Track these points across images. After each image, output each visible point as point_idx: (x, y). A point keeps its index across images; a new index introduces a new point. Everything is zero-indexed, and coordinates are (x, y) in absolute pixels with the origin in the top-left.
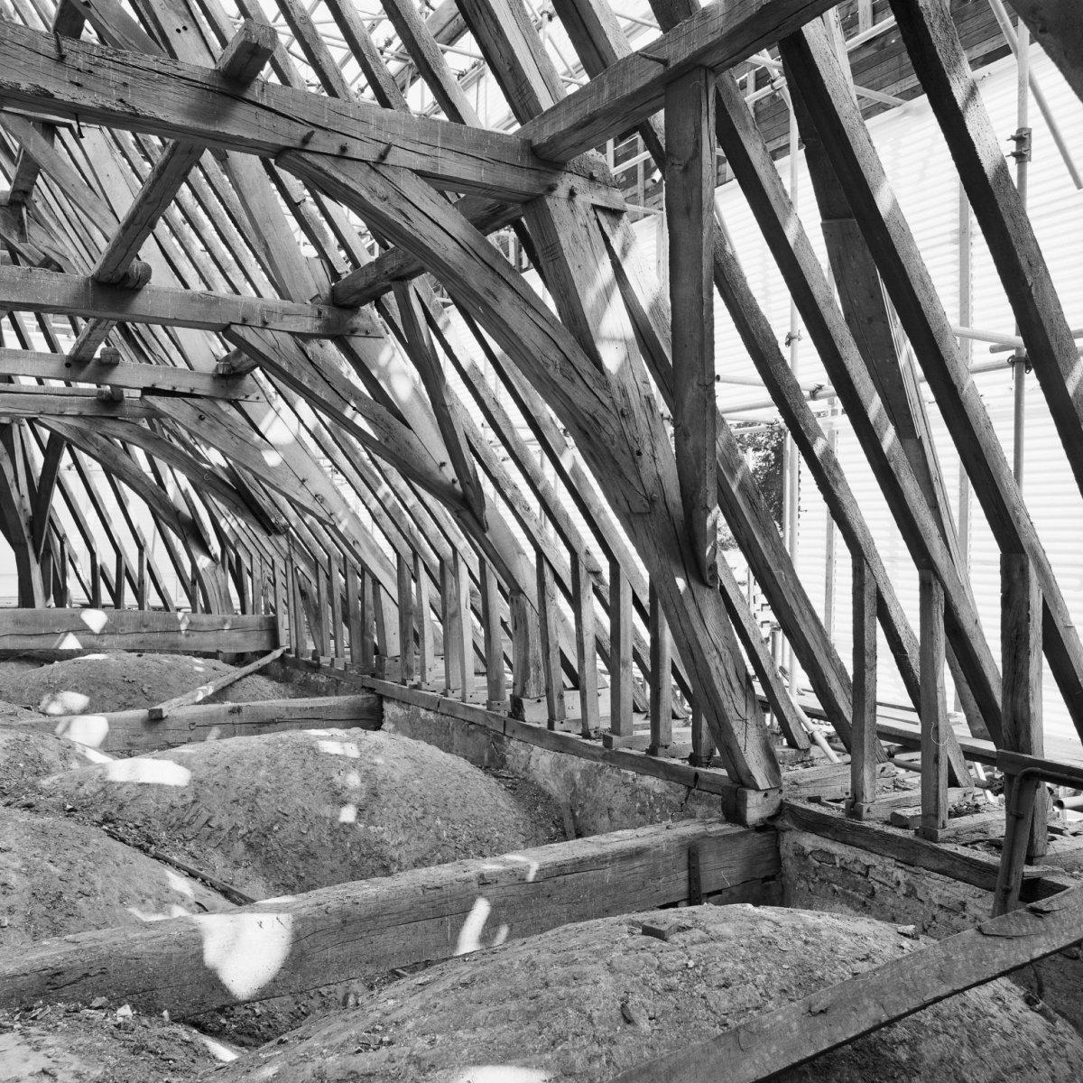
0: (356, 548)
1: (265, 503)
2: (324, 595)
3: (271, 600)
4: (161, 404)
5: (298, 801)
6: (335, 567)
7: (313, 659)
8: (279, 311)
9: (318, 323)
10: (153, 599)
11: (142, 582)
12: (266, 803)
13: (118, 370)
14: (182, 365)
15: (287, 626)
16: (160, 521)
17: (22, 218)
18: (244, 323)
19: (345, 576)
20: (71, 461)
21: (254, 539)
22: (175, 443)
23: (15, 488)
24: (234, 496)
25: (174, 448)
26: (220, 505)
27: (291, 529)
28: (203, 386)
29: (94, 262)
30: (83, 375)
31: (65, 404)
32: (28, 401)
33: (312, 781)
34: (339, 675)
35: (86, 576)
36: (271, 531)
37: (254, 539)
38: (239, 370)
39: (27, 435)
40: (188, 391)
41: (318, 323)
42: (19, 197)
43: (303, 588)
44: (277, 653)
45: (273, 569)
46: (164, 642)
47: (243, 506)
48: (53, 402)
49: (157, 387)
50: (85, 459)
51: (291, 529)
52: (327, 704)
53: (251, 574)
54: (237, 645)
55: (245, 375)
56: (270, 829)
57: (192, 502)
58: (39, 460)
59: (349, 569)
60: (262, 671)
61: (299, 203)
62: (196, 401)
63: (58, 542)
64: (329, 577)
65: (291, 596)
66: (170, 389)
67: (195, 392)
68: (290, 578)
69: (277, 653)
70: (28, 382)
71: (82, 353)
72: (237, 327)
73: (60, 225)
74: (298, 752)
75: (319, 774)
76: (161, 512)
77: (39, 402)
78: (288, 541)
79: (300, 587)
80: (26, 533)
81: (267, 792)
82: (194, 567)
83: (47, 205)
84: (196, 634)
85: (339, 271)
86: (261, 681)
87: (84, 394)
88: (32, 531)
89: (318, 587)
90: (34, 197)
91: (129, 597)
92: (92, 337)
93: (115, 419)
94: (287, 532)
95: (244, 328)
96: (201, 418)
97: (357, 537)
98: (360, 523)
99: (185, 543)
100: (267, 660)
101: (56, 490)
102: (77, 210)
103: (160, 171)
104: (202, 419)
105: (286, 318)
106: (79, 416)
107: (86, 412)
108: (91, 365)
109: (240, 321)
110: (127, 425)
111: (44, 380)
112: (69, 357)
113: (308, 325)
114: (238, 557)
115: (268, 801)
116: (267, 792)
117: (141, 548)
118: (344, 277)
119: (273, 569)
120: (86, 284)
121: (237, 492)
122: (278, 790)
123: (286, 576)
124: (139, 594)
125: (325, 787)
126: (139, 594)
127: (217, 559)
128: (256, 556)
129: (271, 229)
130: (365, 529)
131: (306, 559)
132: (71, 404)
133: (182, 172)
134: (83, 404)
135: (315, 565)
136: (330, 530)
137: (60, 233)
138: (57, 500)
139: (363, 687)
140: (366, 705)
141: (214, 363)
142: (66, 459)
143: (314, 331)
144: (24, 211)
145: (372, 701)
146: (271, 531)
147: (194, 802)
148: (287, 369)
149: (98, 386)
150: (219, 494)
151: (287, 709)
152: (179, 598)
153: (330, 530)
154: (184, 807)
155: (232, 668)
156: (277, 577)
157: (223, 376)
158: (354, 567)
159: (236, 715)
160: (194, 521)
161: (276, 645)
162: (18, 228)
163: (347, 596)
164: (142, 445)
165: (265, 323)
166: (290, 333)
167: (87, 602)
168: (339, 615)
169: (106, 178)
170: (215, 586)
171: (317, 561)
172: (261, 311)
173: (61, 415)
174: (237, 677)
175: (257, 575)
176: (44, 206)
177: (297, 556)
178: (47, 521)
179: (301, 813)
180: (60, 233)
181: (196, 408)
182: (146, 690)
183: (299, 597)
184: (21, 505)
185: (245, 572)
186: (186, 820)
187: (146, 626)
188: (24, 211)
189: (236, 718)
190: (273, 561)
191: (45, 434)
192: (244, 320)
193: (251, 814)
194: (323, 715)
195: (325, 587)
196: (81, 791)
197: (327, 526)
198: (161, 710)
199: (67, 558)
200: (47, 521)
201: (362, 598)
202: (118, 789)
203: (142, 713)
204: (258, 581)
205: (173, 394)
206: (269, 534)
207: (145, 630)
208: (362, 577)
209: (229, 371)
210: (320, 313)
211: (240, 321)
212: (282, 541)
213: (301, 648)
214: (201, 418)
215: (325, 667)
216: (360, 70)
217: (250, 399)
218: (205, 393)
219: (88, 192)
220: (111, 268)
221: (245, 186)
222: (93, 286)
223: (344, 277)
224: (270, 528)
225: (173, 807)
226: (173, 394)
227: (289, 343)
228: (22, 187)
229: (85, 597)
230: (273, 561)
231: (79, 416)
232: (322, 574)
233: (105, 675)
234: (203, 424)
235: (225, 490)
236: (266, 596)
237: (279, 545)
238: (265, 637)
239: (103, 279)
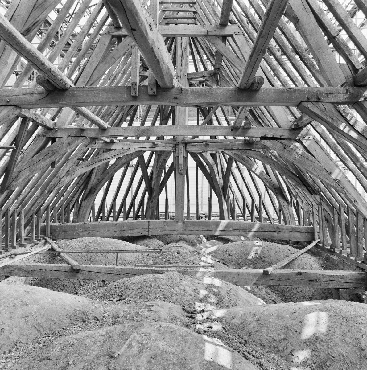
0: (356, 204)
1: (310, 181)
2: (337, 221)
3: (311, 220)
4: (267, 143)
5: (340, 349)
6: (342, 210)
7: (331, 248)
8: (326, 92)
9: (346, 96)
10: (264, 215)
11: (261, 210)
12: (322, 347)
13: (251, 130)
14: (275, 126)
15: (318, 231)
16: (267, 187)
17: (218, 79)
18: (308, 100)
19: (348, 215)
20: (236, 166)
21: (304, 195)
22: (273, 158)
23: (218, 176)
24: (297, 179)
25: (273, 160)
26: (290, 182)
27: (321, 192)
28: (285, 134)
29: (238, 83)
30: (237, 133)
31: (233, 145)
32: (221, 145)
33: (347, 339)
34: (345, 259)
35: (241, 206)
36: (313, 193)
37: (304, 195)
38: (301, 126)
39: (222, 157)
40: (279, 137)
41: (346, 96)
42: (217, 71)
43: (327, 218)
44: (314, 244)
45: (312, 208)
46: (269, 235)
47: (301, 183)
48: (228, 145)
49: (267, 136)
50: (241, 165)
51: (321, 192)
52: (341, 275)
53: (303, 209)
54: (297, 238)
55: (303, 128)
56: (325, 363)
57: (279, 180)
58: (225, 165)
59: (350, 212)
60: (309, 251)
61: (336, 37)
62: (283, 141)
63: (232, 194)
64: (339, 215)
65: (321, 219)
66: (272, 136)
67: (275, 136)
68: (320, 212)
69: (314, 244)
70: (221, 138)
71: (237, 125)
72: (305, 102)
73: (231, 79)
74: (337, 318)
75: (350, 335)
76: (268, 184)
77: (224, 145)
78: (320, 197)
79: (325, 217)
80: (221, 192)
81: (322, 341)
82: (280, 205)
83: (226, 73)
84: (281, 233)
85: (358, 68)
86: (308, 256)
87: (240, 141)
88: (223, 191)
89: (334, 218)
90: (222, 71)
91: (256, 214)
92: (240, 117)
93: (250, 150)
94: (320, 194)
95: (308, 103)
96: (285, 148)
97: (356, 199)
98: (358, 192)
99: (277, 196)
100: (310, 247)
101: (231, 176)
102: (232, 66)
103: (267, 40)
104: (285, 148)
105: (329, 96)
106: (238, 149)
107: (240, 148)
108: (240, 129)
109: (306, 100)
110: (256, 152)
111: (227, 137)
112: (232, 127)
113: (342, 97)
114: (297, 202)
115: (323, 346)
116: (322, 341)
117: (260, 197)
118: (360, 71)
119: (312, 208)
120: (235, 91)
121: (298, 177)
122: (328, 340)
123: (318, 211)
124: (259, 213)
125: (354, 343)
126: (259, 213)
127: (289, 202)
128: (305, 201)
129: (321, 52)
130: (360, 195)
131: (328, 205)
132: (235, 145)
133: (281, 10)
134: (239, 145)
135: (332, 208)
136: (342, 196)
137: (231, 82)
138: (231, 179)
139: (358, 267)
140: (360, 277)
141: (289, 125)
142: (234, 165)
143: (344, 101)
144: (218, 76)
145: (363, 275)
146: (313, 193)
147: (284, 339)
148: (330, 121)
149: (245, 138)
150: (290, 177)
151: (322, 275)
152: (274, 216)
153: (342, 196)
154: (279, 341)
155: (296, 250)
156: (314, 211)
157: (294, 129)
158: (352, 211)
159: (299, 276)
160: (280, 187)
161: (314, 240)
162: (217, 83)
163: (349, 224)
164: (260, 159)
165: (319, 99)
166: (331, 103)
167: (241, 215)
168: (344, 231)
169: (245, 53)
170: (288, 213)
171: (333, 207)
172: (317, 93)
173: (231, 150)
174: (299, 255)
175: (305, 209)
176: (225, 73)
177: (324, 204)
178: (228, 187)
179: (342, 358)
180: (231, 82)
181: (282, 144)
182: (262, 257)
183: (324, 221)
184: (220, 182)
185: (300, 208)
186: (281, 349)
187: (262, 229)
188: (218, 76)
189: (299, 277)
190: (312, 205)
191: (227, 157)
192: (308, 99)
193: (314, 352)
194: (340, 280)
195: (337, 218)
196: (233, 321)
197: (341, 194)
198: (268, 271)
199: (235, 200)
200: (228, 187)
201: (357, 226)
202: (249, 324)
203: (261, 271)
204: (306, 212)
205: (273, 138)
206: (312, 194)
207: (262, 230)
208: (357, 216)
209: (297, 127)
210: (347, 91)
211: (306, 100)
212: (318, 198)
213: (325, 243)
214: (285, 148)
215: (337, 253)
216: (219, 211)
217: (305, 138)
218: (286, 137)
219: (237, 60)
220: (245, 81)
221: (307, 33)
222: (238, 91)
223: (360, 71)
224: (312, 191)
225: (274, 340)
226: (273, 138)
227: (330, 107)
228: (218, 66)
229: (240, 213)
230: (312, 205)
231: (238, 149)
232: (335, 212)
233: (246, 250)
234: (285, 150)
235: (293, 176)
236: (309, 218)
237: (316, 199)
238: (309, 236)
239: (242, 87)
